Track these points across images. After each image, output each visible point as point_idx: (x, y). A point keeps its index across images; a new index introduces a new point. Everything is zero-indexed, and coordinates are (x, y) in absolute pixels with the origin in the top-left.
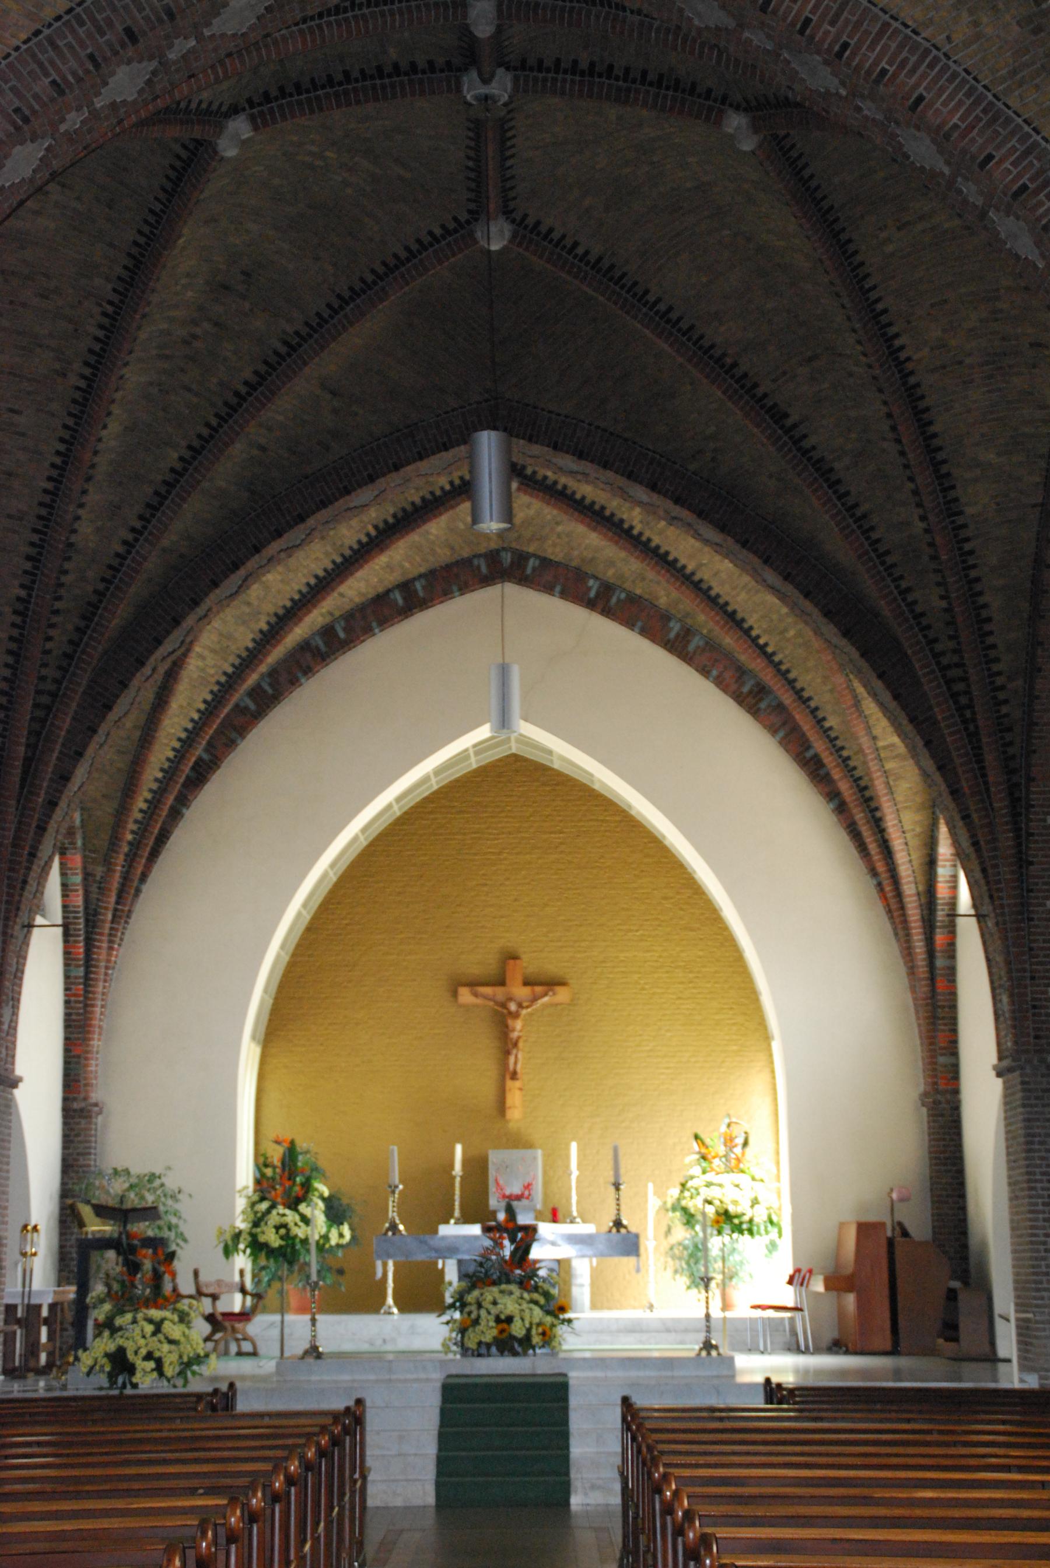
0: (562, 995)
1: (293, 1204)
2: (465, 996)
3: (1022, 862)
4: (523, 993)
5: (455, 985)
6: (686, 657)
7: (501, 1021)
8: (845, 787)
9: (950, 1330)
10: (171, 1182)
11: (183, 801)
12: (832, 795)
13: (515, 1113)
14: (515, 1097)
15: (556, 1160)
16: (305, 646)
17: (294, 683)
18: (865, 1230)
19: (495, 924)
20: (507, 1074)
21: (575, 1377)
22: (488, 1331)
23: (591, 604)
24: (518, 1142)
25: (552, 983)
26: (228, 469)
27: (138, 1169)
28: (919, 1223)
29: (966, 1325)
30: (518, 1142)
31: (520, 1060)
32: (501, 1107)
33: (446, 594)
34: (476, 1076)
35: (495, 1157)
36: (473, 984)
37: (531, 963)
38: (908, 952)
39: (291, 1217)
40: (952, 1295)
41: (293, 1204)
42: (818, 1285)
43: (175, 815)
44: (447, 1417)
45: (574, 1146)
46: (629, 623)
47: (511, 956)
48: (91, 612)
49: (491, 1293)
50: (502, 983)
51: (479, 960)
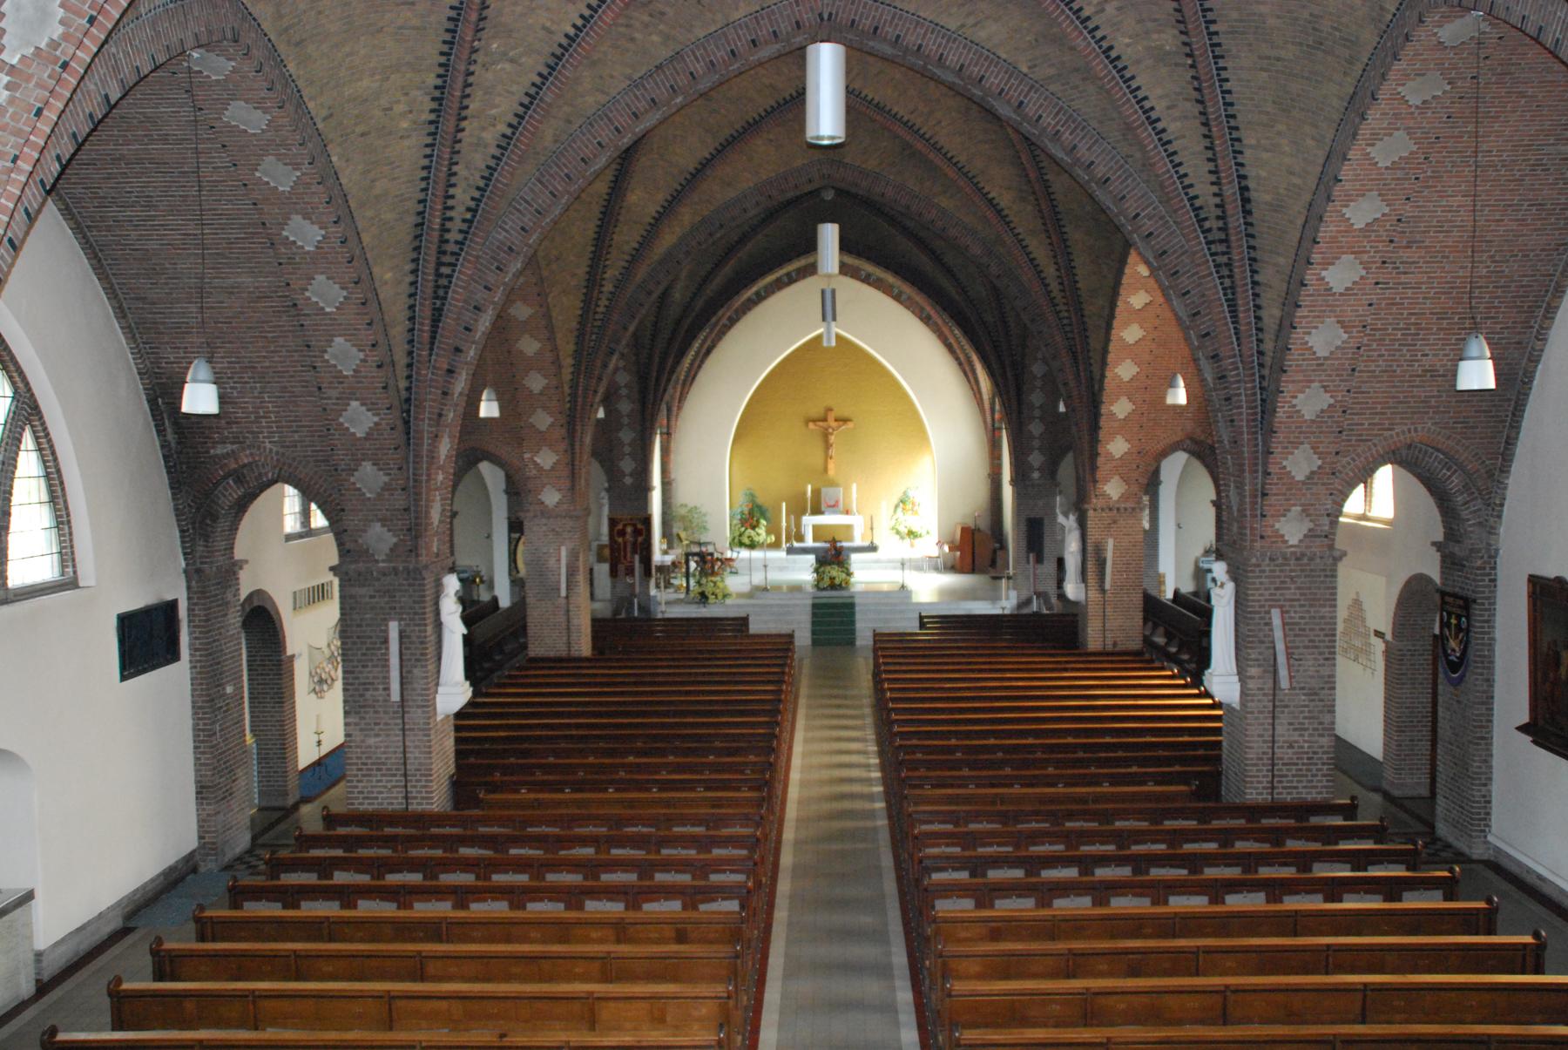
0: (850, 425)
1: (753, 528)
2: (811, 425)
3: (1020, 412)
4: (834, 424)
5: (808, 421)
6: (901, 303)
7: (826, 436)
8: (961, 357)
9: (993, 563)
10: (703, 510)
11: (702, 362)
12: (957, 359)
13: (832, 472)
14: (831, 465)
15: (847, 489)
16: (749, 300)
17: (744, 313)
18: (963, 530)
19: (823, 406)
20: (827, 457)
21: (857, 600)
22: (827, 582)
23: (863, 281)
24: (833, 484)
25: (845, 420)
26: (728, 269)
27: (691, 505)
28: (984, 524)
29: (999, 562)
30: (833, 484)
31: (833, 452)
32: (826, 470)
33: (804, 277)
34: (815, 455)
35: (824, 490)
36: (814, 421)
37: (839, 411)
38: (985, 422)
39: (752, 533)
40: (995, 551)
41: (753, 528)
42: (946, 548)
43: (700, 367)
44: (814, 615)
45: (854, 486)
46: (878, 288)
47: (830, 410)
48: (678, 322)
49: (828, 568)
50: (825, 420)
51: (816, 410)
